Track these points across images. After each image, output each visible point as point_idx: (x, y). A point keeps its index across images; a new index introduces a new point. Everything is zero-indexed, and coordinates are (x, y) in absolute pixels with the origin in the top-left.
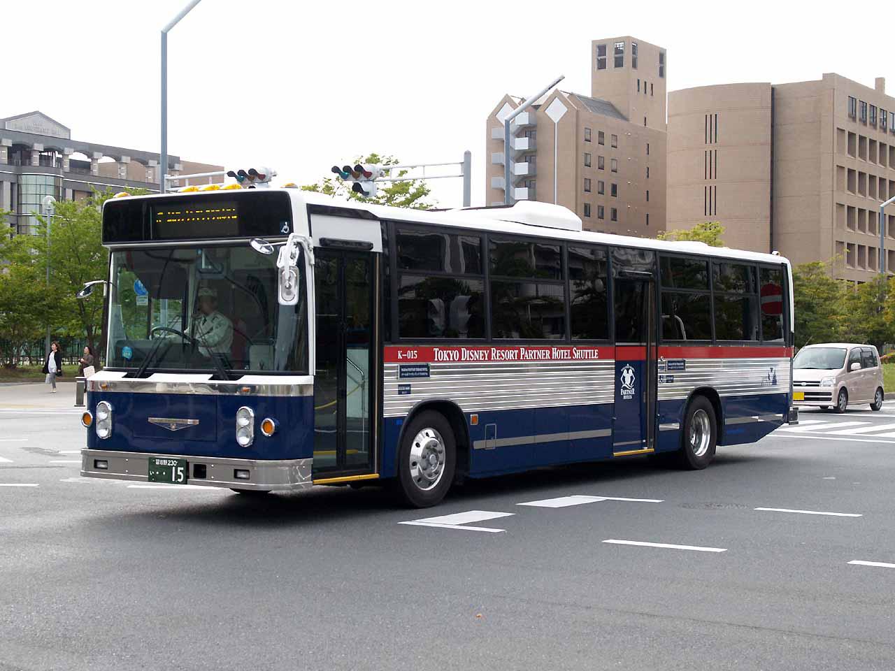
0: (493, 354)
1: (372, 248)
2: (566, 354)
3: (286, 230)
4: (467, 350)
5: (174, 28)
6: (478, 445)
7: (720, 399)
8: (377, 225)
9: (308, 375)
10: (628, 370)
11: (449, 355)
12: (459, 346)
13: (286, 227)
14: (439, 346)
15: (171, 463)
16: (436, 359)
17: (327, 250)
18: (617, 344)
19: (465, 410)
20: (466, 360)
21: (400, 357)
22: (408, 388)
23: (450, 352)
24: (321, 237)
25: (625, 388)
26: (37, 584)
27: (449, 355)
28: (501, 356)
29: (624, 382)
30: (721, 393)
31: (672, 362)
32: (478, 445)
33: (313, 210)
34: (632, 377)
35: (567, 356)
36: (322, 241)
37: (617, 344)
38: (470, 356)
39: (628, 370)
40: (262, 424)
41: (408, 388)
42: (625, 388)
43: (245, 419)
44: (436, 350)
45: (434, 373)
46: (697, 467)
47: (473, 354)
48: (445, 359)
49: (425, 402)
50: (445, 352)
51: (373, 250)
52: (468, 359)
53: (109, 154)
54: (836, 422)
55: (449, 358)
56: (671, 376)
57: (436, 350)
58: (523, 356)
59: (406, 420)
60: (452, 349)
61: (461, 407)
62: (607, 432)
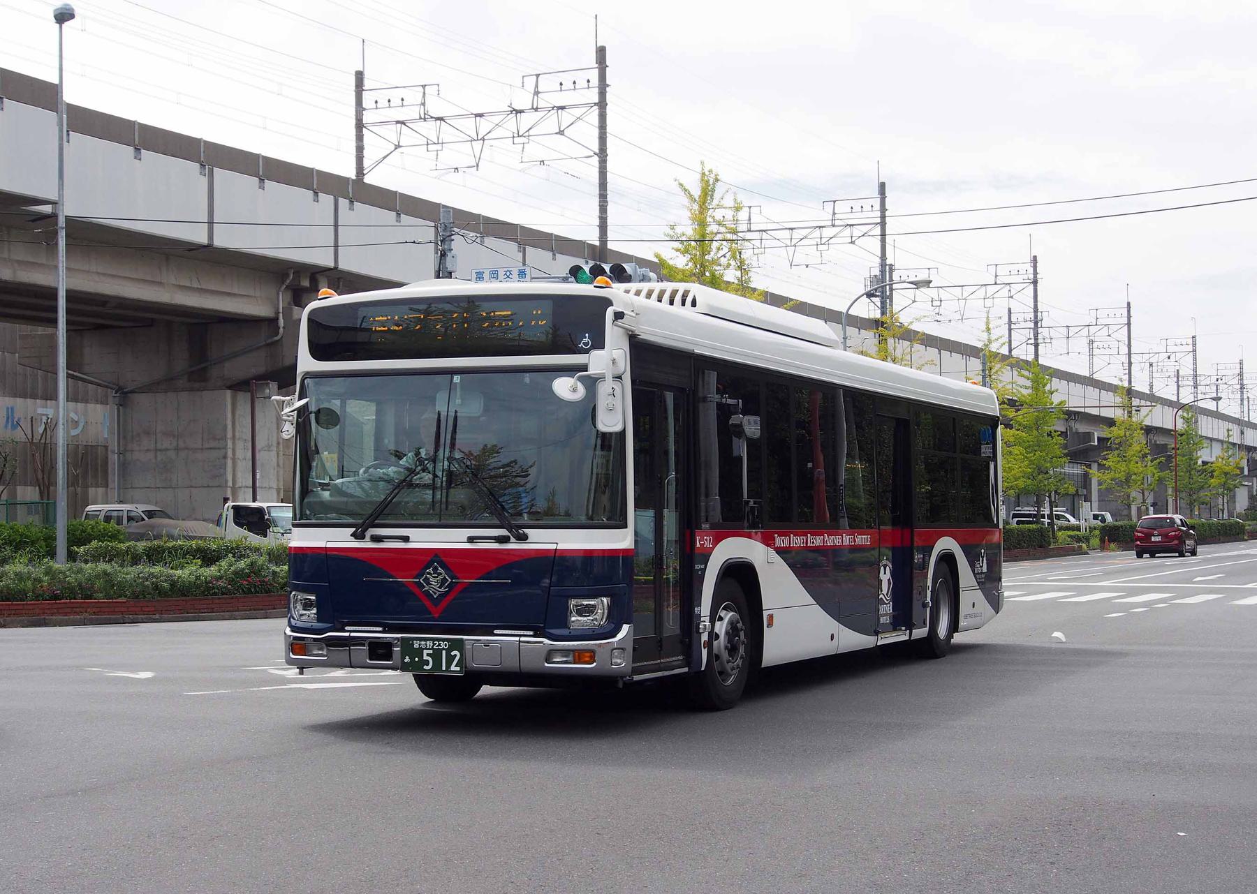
15: (439, 645)
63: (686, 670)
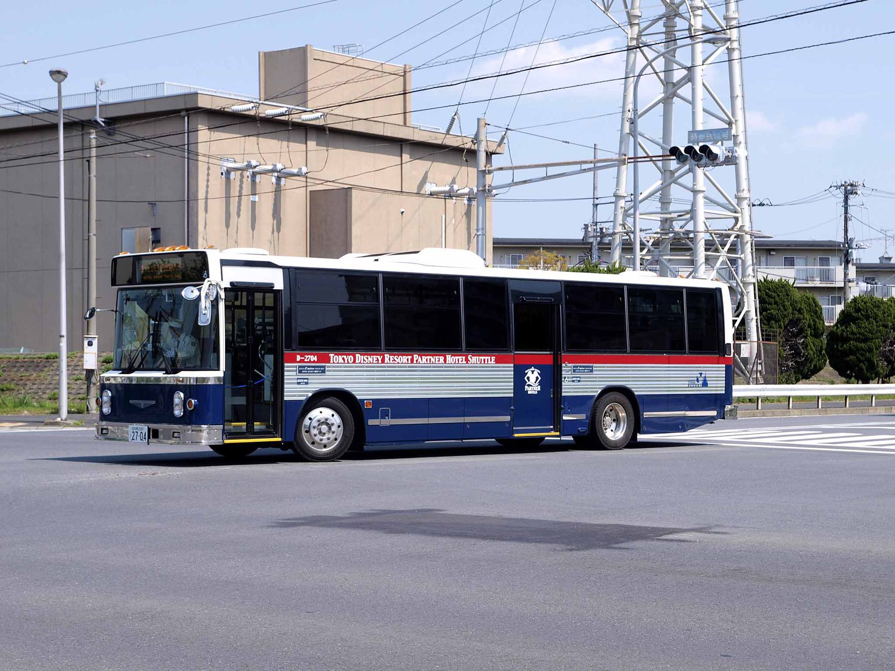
0: (415, 359)
1: (274, 287)
2: (460, 360)
3: (205, 276)
4: (361, 355)
5: (644, 57)
6: (371, 422)
7: (636, 397)
8: (280, 272)
9: (219, 370)
10: (533, 372)
11: (343, 359)
12: (444, 353)
13: (205, 274)
14: (418, 353)
16: (332, 361)
17: (235, 289)
18: (515, 352)
19: (358, 397)
20: (360, 363)
21: (298, 360)
22: (306, 381)
23: (345, 357)
24: (231, 281)
25: (529, 385)
26: (505, 597)
27: (343, 359)
28: (394, 360)
29: (529, 381)
30: (637, 391)
31: (577, 367)
32: (371, 422)
33: (224, 263)
34: (537, 378)
35: (462, 361)
36: (232, 283)
37: (515, 352)
38: (364, 360)
39: (533, 372)
40: (187, 402)
41: (306, 381)
42: (529, 385)
43: (179, 396)
44: (332, 355)
45: (595, 371)
46: (609, 448)
47: (367, 358)
48: (340, 362)
49: (322, 390)
50: (340, 356)
51: (274, 289)
52: (362, 362)
53: (333, 191)
54: (673, 415)
55: (344, 361)
56: (305, 379)
57: (332, 355)
58: (417, 361)
59: (303, 405)
60: (347, 355)
61: (355, 395)
62: (507, 418)
63: (255, 370)
